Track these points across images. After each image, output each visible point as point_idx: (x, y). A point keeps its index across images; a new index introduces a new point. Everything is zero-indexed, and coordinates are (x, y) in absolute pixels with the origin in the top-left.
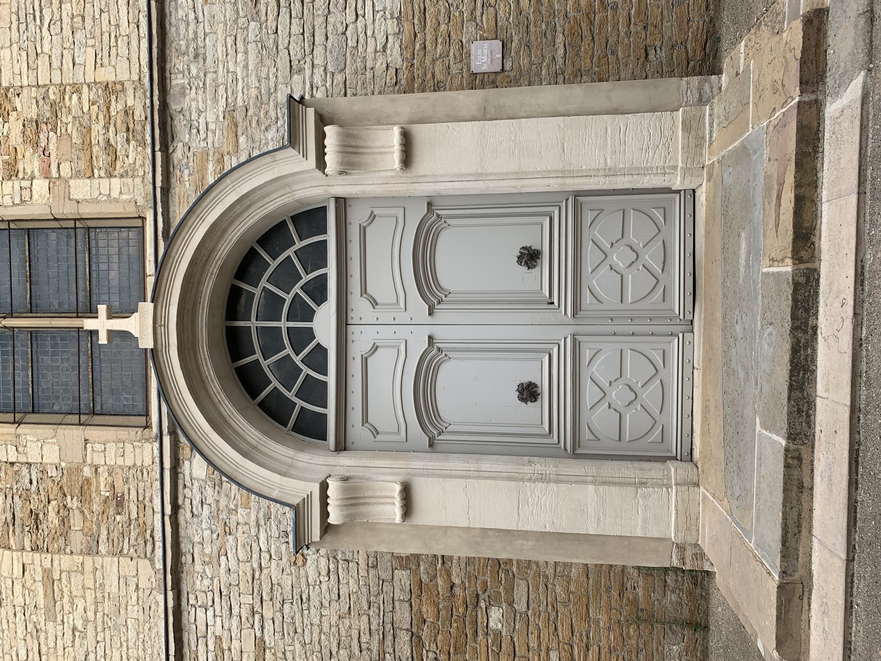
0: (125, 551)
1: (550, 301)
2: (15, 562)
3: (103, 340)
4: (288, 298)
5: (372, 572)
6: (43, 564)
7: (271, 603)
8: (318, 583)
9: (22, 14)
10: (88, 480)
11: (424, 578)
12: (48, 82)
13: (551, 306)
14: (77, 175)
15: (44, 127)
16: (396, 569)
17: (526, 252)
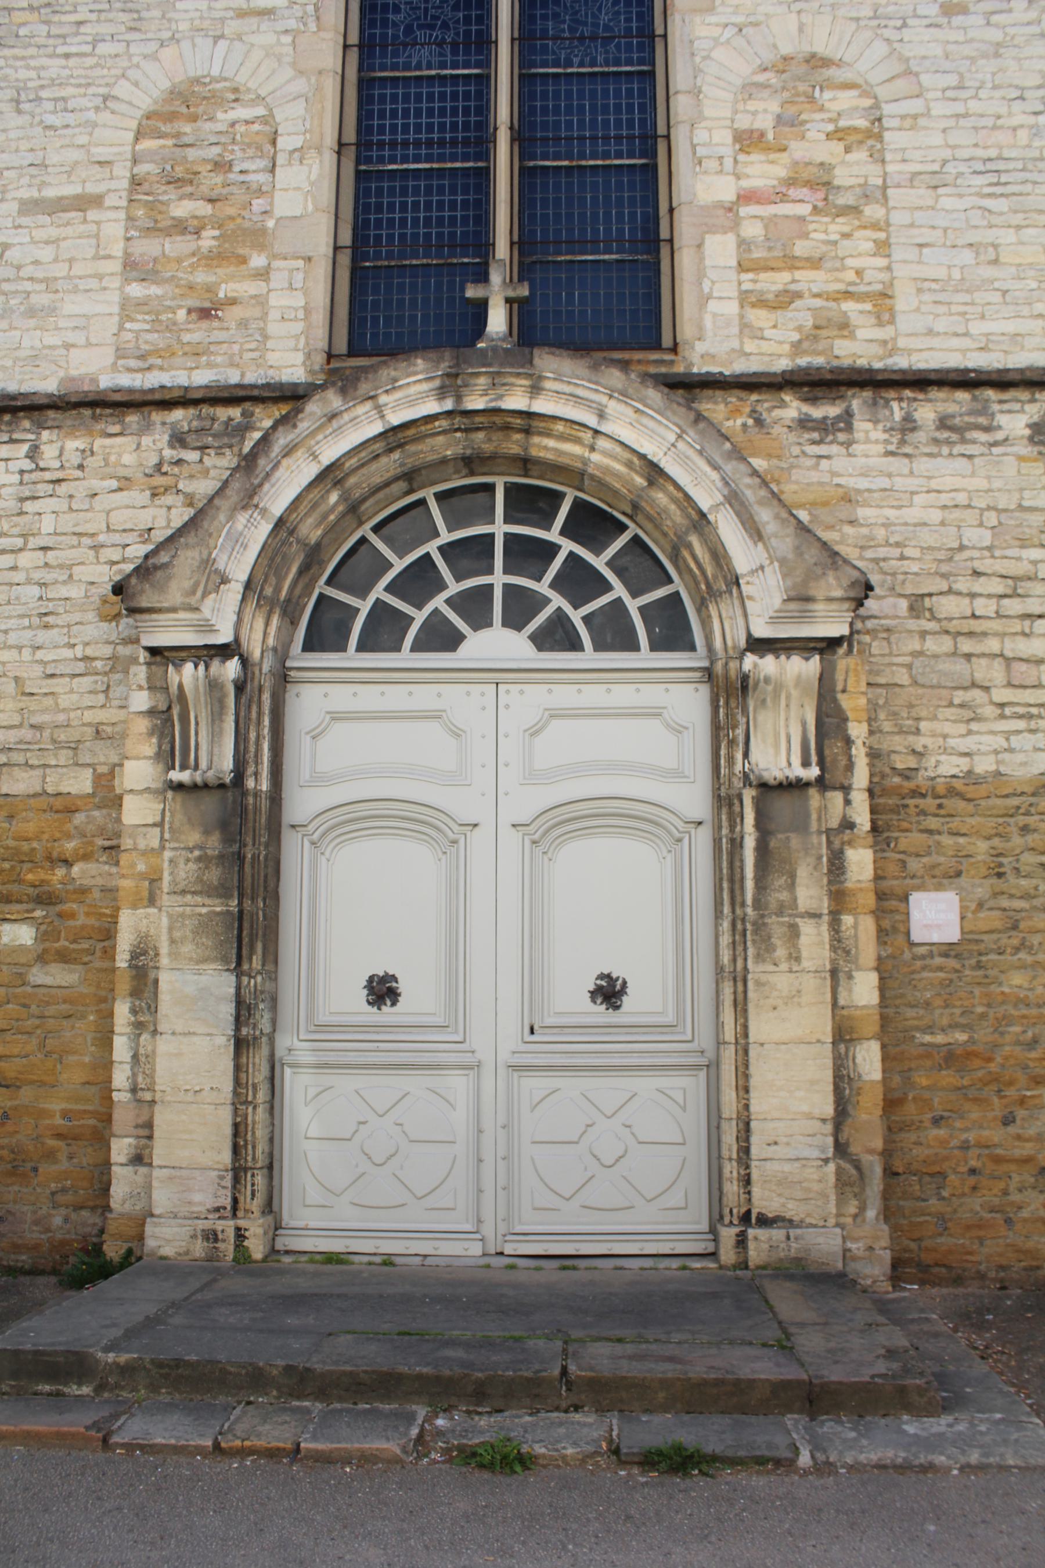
0: (128, 325)
1: (536, 1028)
2: (115, 150)
3: (472, 292)
4: (543, 587)
5: (90, 731)
6: (111, 195)
7: (42, 564)
8: (72, 641)
9: (1001, 166)
10: (243, 260)
11: (79, 818)
12: (891, 203)
13: (527, 1030)
14: (744, 245)
15: (821, 195)
16: (95, 770)
17: (618, 987)
